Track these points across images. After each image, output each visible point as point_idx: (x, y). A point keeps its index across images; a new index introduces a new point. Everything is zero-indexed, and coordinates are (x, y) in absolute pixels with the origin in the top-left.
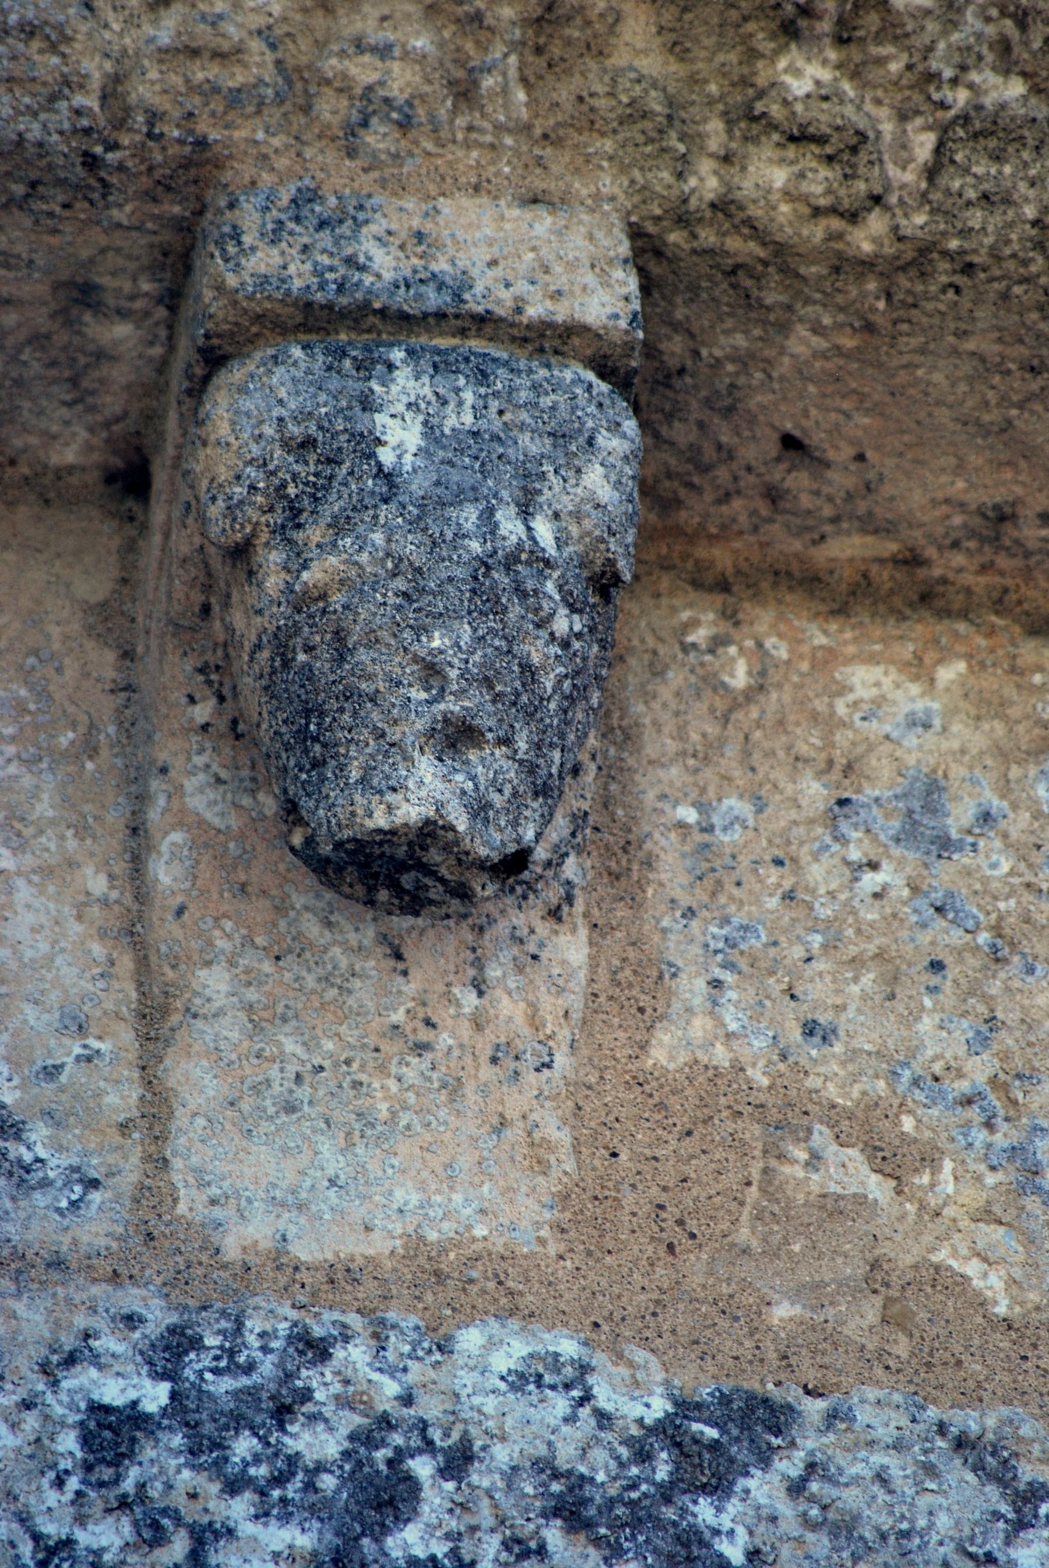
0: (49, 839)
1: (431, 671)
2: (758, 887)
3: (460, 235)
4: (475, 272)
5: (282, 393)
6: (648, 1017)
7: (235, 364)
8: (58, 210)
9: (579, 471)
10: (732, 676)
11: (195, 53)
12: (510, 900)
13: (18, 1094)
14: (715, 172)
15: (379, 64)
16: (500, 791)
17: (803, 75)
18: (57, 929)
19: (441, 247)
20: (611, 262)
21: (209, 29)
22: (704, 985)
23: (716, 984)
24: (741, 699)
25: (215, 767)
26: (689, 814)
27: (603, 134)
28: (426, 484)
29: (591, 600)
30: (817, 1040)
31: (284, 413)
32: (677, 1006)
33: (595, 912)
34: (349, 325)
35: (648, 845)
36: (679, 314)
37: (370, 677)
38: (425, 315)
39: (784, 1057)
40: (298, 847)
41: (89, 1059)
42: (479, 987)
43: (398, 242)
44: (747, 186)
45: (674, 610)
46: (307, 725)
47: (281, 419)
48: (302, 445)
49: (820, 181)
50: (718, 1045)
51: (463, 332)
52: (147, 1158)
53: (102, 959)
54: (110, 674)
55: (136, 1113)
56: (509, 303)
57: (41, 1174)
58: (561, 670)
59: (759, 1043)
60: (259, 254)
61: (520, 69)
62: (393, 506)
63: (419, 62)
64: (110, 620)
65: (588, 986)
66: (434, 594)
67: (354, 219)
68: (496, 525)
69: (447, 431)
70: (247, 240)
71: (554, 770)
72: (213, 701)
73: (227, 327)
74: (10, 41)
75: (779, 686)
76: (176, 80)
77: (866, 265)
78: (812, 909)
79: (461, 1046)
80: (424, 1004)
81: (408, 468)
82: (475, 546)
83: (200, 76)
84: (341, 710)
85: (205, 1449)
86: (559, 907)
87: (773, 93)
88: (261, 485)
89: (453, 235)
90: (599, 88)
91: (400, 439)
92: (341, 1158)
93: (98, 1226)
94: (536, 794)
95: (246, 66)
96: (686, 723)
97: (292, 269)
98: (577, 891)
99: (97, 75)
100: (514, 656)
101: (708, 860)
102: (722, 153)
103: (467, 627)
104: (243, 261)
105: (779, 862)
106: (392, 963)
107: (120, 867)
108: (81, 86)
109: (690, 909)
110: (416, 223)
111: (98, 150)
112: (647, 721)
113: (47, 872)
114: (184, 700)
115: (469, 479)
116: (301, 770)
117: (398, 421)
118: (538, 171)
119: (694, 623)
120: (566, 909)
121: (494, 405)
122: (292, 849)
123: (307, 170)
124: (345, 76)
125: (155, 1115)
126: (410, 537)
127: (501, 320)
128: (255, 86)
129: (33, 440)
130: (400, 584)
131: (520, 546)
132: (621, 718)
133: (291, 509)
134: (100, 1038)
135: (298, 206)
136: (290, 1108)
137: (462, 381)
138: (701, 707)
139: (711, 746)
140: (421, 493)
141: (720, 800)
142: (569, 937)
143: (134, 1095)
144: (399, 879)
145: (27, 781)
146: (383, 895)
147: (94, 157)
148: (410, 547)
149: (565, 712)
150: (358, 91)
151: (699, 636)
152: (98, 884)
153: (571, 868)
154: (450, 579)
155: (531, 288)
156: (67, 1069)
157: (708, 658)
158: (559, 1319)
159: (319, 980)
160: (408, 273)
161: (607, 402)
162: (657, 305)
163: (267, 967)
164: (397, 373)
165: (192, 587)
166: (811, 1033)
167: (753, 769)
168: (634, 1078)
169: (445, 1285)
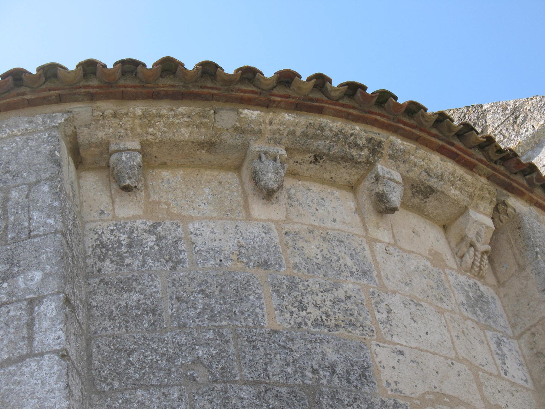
6: (149, 198)
17: (151, 130)
34: (119, 151)
49: (153, 137)
64: (108, 176)
77: (157, 143)
85: (119, 231)
91: (124, 158)
93: (110, 217)
125: (114, 209)
144: (127, 189)
148: (125, 165)
158: (144, 219)
169: (135, 218)
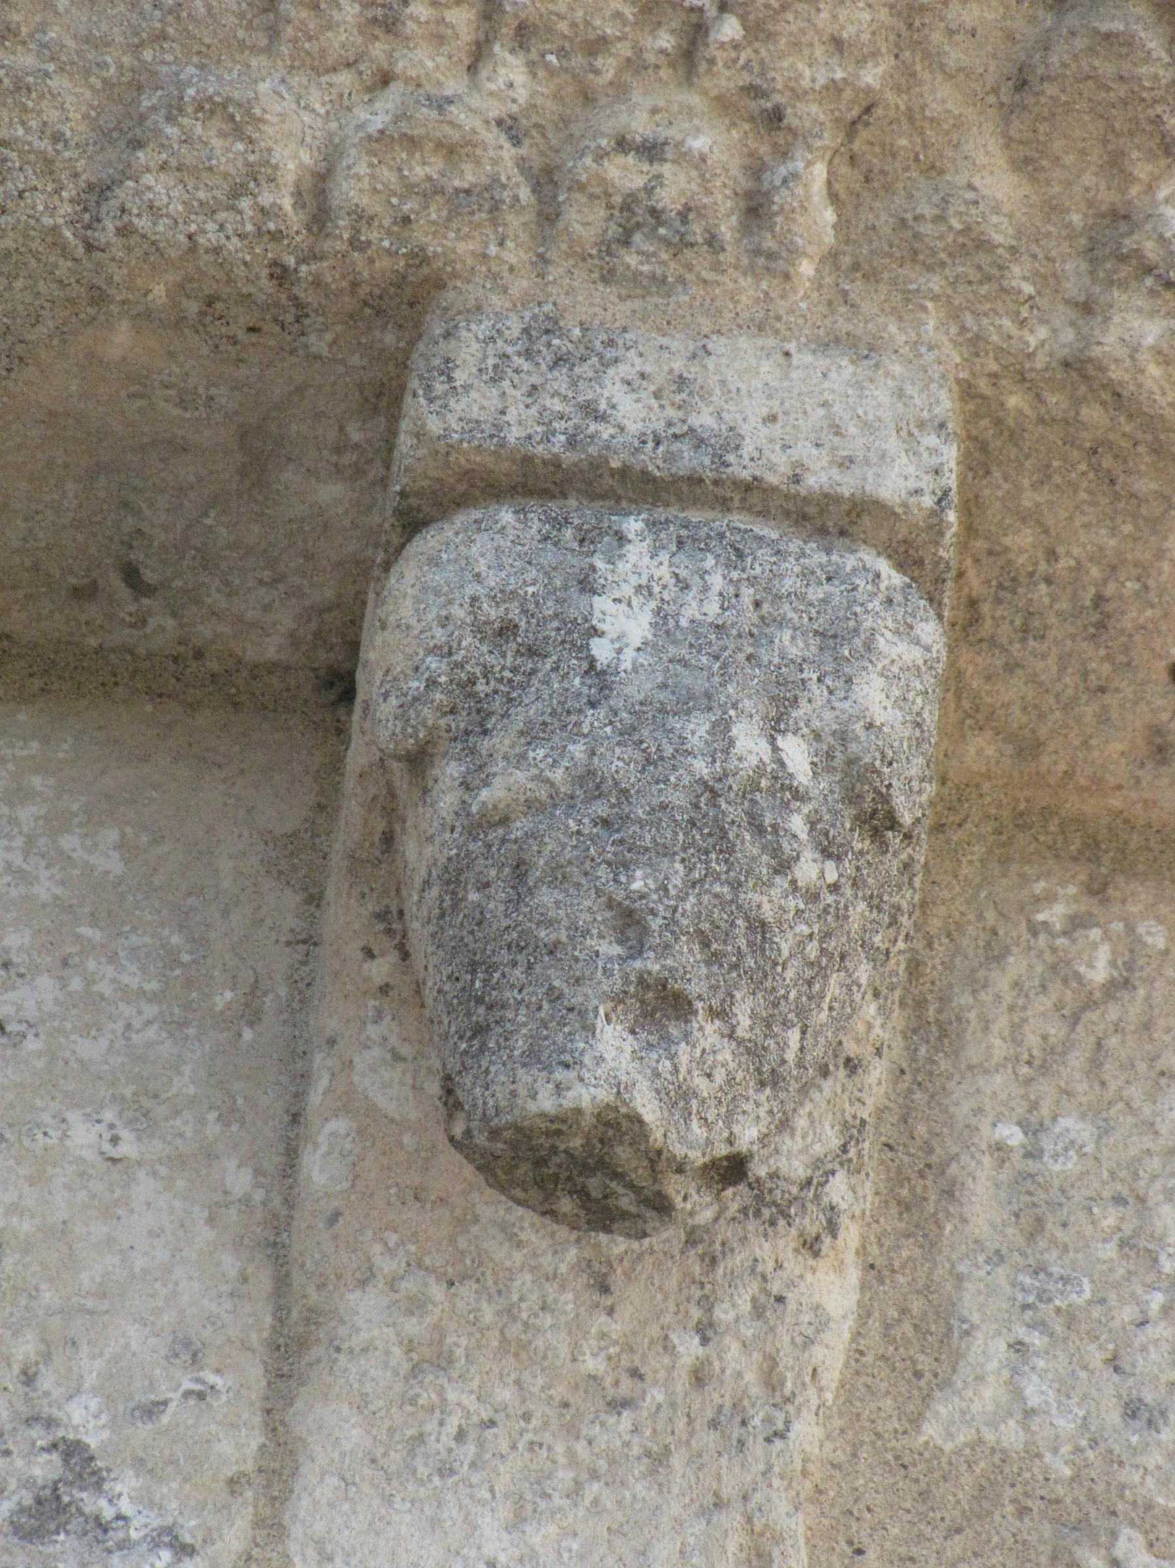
0: (186, 1123)
1: (629, 922)
2: (1089, 1230)
3: (734, 382)
4: (745, 429)
5: (482, 567)
7: (433, 530)
8: (241, 335)
9: (849, 681)
10: (1091, 966)
11: (413, 143)
12: (752, 1225)
13: (105, 1435)
14: (1072, 324)
15: (646, 167)
16: (709, 1076)
18: (181, 1233)
19: (705, 394)
20: (921, 425)
21: (434, 114)
22: (1003, 1347)
23: (1018, 1347)
24: (1097, 994)
25: (394, 1040)
26: (1013, 1135)
27: (929, 268)
28: (648, 686)
29: (857, 846)
30: (1138, 1424)
31: (479, 590)
32: (964, 1371)
33: (874, 1250)
34: (580, 486)
35: (953, 1169)
36: (1028, 500)
37: (550, 923)
38: (676, 479)
39: (1094, 1443)
40: (458, 1137)
41: (201, 1396)
42: (705, 1331)
43: (652, 388)
44: (1109, 342)
45: (1024, 880)
46: (473, 982)
47: (474, 599)
48: (501, 632)
50: (1012, 1423)
51: (725, 505)
52: (259, 1523)
53: (233, 1273)
54: (291, 922)
55: (250, 1466)
56: (784, 469)
57: (121, 1535)
58: (804, 929)
59: (1066, 1425)
60: (474, 394)
61: (829, 183)
62: (602, 712)
63: (697, 167)
65: (853, 1340)
66: (640, 823)
67: (601, 357)
68: (732, 742)
69: (684, 623)
70: (460, 377)
71: (790, 1056)
72: (393, 957)
73: (425, 483)
74: (185, 121)
75: (1149, 981)
76: (388, 175)
78: (1156, 1260)
79: (673, 1405)
80: (631, 1350)
81: (627, 665)
82: (701, 767)
83: (420, 172)
84: (514, 964)
86: (817, 1238)
87: (1148, 227)
88: (443, 679)
89: (723, 382)
90: (927, 210)
91: (623, 628)
92: (505, 1535)
94: (762, 1084)
95: (478, 162)
96: (1025, 1020)
97: (512, 415)
98: (844, 1220)
99: (291, 166)
100: (739, 907)
101: (1030, 1194)
102: (1082, 299)
103: (678, 866)
104: (452, 403)
105: (1119, 1200)
106: (596, 1297)
107: (273, 1160)
108: (271, 180)
109: (997, 1252)
110: (678, 365)
111: (291, 261)
112: (972, 1015)
113: (180, 1162)
114: (360, 955)
115: (700, 684)
116: (461, 1038)
117: (623, 607)
118: (843, 309)
119: (1049, 898)
120: (827, 1240)
121: (748, 593)
122: (452, 1139)
123: (549, 295)
124: (602, 181)
126: (618, 750)
127: (774, 489)
128: (487, 188)
129: (225, 629)
130: (601, 809)
131: (760, 770)
132: (940, 1011)
133: (479, 711)
134: (218, 1371)
135: (530, 338)
136: (447, 1471)
137: (710, 562)
138: (1044, 1003)
139: (1053, 1052)
140: (641, 697)
141: (1054, 1119)
142: (832, 1277)
143: (254, 1445)
145: (167, 1048)
146: (566, 1205)
147: (285, 268)
148: (619, 763)
149: (810, 983)
150: (618, 200)
151: (1054, 914)
152: (240, 1181)
153: (838, 1189)
154: (664, 807)
155: (815, 452)
156: (172, 1406)
157: (1061, 942)
159: (499, 1313)
160: (660, 426)
161: (898, 598)
162: (998, 487)
163: (437, 1291)
164: (629, 547)
165: (370, 810)
166: (1134, 1415)
167: (1103, 1084)
168: (897, 1458)
